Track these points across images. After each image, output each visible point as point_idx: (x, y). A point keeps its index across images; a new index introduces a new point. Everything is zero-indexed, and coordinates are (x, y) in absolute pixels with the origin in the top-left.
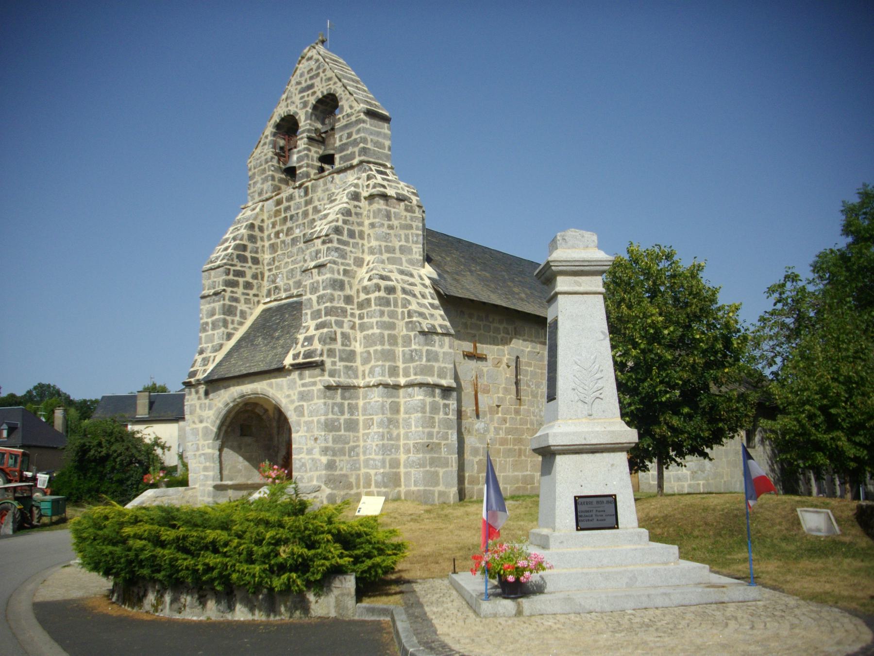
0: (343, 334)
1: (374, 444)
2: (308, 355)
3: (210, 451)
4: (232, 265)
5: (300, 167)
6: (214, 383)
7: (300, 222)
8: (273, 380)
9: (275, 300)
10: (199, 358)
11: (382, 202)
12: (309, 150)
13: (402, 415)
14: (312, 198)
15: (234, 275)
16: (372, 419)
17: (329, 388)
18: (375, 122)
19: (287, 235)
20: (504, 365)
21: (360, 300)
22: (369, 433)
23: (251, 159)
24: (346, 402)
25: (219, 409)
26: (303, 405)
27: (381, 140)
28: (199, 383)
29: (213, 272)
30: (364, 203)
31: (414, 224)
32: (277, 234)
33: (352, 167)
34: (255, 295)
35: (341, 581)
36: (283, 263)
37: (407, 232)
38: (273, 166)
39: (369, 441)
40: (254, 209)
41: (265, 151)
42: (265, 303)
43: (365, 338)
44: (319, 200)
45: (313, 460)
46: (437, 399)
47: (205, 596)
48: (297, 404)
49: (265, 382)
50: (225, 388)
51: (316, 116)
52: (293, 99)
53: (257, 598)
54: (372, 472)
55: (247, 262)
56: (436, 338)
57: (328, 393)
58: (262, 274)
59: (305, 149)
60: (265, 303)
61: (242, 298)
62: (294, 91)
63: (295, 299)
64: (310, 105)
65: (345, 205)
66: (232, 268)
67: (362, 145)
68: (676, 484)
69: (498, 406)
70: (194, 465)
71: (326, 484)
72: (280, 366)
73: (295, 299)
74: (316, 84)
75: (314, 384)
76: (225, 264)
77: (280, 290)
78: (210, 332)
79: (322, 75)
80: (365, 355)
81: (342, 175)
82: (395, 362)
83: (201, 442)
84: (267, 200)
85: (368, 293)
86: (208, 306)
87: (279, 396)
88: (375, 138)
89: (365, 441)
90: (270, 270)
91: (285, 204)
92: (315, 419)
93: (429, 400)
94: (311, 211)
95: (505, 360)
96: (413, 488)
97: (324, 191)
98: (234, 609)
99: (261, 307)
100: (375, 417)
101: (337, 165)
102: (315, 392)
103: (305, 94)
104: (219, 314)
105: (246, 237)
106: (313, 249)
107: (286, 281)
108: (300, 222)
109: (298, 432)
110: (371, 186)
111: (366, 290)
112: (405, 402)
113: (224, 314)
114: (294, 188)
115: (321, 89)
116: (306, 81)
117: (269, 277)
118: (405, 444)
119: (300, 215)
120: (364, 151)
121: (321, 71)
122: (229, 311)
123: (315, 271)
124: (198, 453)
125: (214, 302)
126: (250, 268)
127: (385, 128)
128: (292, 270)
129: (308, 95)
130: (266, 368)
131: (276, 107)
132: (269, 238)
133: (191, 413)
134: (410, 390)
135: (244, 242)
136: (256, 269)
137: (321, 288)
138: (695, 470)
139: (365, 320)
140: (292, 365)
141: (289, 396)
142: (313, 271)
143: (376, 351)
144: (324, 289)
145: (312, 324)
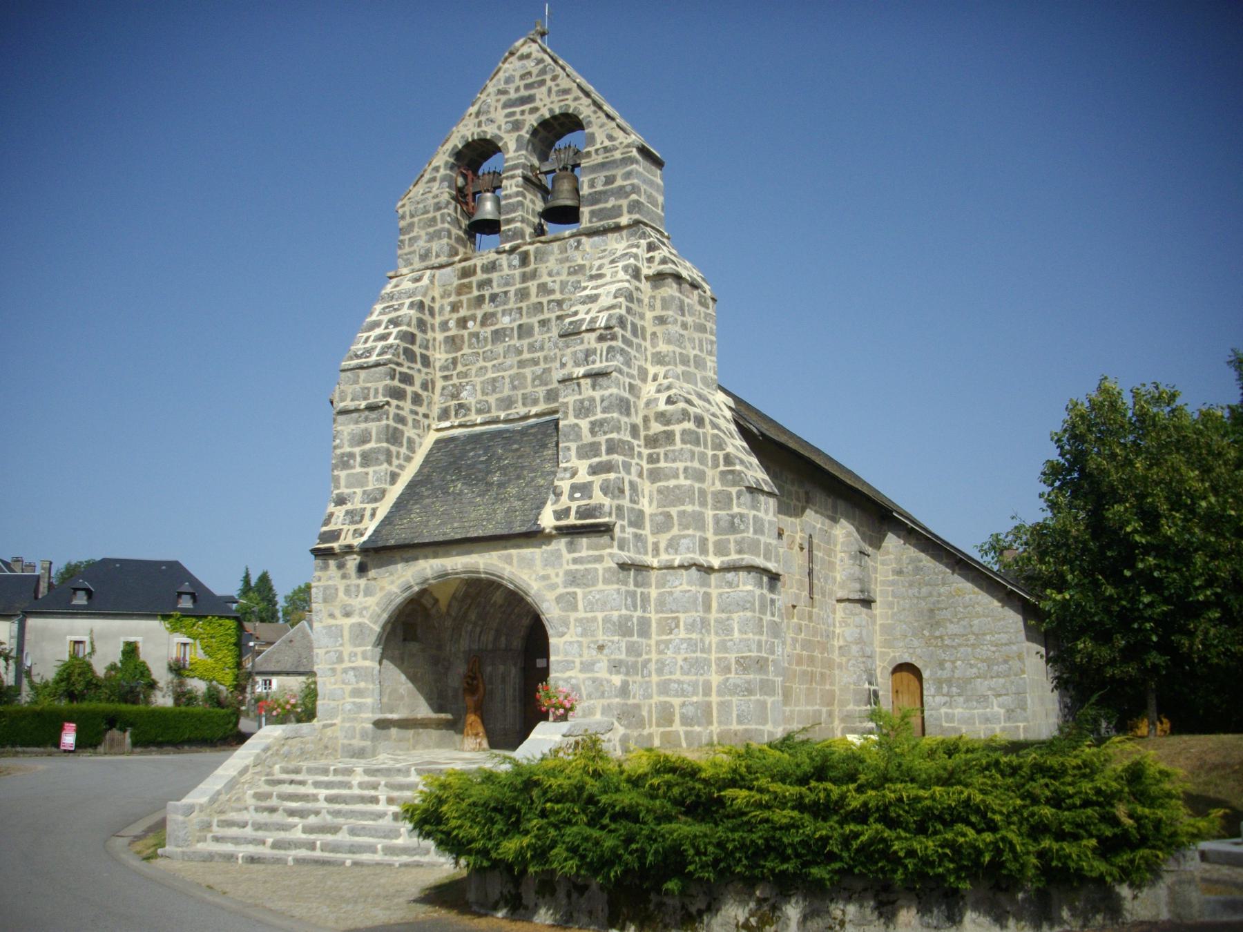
0: (631, 482)
1: (680, 658)
2: (582, 514)
3: (368, 663)
4: (398, 364)
5: (509, 222)
6: (377, 554)
7: (511, 305)
8: (514, 552)
9: (461, 426)
10: (340, 512)
11: (675, 286)
12: (525, 197)
13: (714, 615)
14: (536, 270)
15: (400, 381)
16: (677, 618)
17: (623, 567)
18: (648, 164)
19: (483, 323)
20: (797, 548)
21: (651, 432)
22: (670, 641)
23: (405, 201)
24: (639, 590)
25: (390, 593)
26: (575, 593)
27: (654, 193)
28: (349, 549)
29: (363, 374)
30: (645, 286)
31: (709, 325)
32: (462, 323)
33: (618, 228)
34: (426, 416)
35: (1177, 861)
36: (474, 369)
37: (701, 335)
38: (449, 215)
39: (669, 653)
40: (417, 280)
41: (435, 190)
42: (438, 430)
43: (659, 491)
44: (550, 274)
45: (594, 680)
46: (765, 591)
47: (893, 903)
48: (561, 590)
49: (495, 554)
50: (407, 561)
51: (533, 145)
52: (492, 115)
53: (1013, 900)
54: (676, 701)
55: (415, 362)
56: (762, 498)
57: (622, 575)
58: (433, 382)
59: (518, 194)
60: (438, 430)
61: (410, 418)
62: (493, 104)
63: (501, 426)
64: (527, 127)
65: (626, 285)
66: (398, 369)
67: (634, 197)
68: (983, 727)
69: (794, 607)
70: (330, 687)
71: (619, 719)
72: (534, 528)
73: (501, 426)
74: (538, 97)
75: (599, 559)
76: (390, 361)
77: (469, 410)
78: (358, 470)
79: (549, 83)
80: (660, 518)
81: (596, 239)
82: (704, 531)
83: (347, 649)
84: (441, 267)
85: (668, 423)
86: (352, 426)
87: (525, 577)
88: (649, 190)
89: (661, 652)
90: (446, 378)
91: (481, 276)
92: (600, 616)
93: (758, 592)
94: (533, 290)
95: (798, 540)
96: (735, 726)
97: (561, 261)
98: (961, 922)
99: (432, 437)
100: (682, 616)
101: (585, 222)
102: (601, 572)
103: (518, 109)
104: (379, 440)
105: (414, 322)
106: (579, 348)
107: (480, 397)
108: (511, 305)
109: (562, 635)
110: (657, 260)
111: (662, 417)
112: (721, 595)
113: (388, 441)
114: (498, 252)
115: (547, 105)
116: (517, 89)
117: (444, 388)
118: (719, 659)
119: (512, 294)
120: (635, 206)
121: (548, 77)
122: (394, 437)
123: (586, 383)
124: (339, 667)
125: (366, 420)
126: (419, 371)
127: (657, 177)
128: (494, 380)
129: (523, 113)
130: (499, 532)
131: (456, 124)
132: (444, 326)
133: (325, 601)
134: (730, 576)
135: (413, 330)
136: (427, 374)
137: (599, 409)
138: (1012, 707)
139: (662, 464)
140: (557, 528)
141: (545, 578)
142: (582, 381)
143: (682, 514)
144: (604, 412)
145: (583, 466)
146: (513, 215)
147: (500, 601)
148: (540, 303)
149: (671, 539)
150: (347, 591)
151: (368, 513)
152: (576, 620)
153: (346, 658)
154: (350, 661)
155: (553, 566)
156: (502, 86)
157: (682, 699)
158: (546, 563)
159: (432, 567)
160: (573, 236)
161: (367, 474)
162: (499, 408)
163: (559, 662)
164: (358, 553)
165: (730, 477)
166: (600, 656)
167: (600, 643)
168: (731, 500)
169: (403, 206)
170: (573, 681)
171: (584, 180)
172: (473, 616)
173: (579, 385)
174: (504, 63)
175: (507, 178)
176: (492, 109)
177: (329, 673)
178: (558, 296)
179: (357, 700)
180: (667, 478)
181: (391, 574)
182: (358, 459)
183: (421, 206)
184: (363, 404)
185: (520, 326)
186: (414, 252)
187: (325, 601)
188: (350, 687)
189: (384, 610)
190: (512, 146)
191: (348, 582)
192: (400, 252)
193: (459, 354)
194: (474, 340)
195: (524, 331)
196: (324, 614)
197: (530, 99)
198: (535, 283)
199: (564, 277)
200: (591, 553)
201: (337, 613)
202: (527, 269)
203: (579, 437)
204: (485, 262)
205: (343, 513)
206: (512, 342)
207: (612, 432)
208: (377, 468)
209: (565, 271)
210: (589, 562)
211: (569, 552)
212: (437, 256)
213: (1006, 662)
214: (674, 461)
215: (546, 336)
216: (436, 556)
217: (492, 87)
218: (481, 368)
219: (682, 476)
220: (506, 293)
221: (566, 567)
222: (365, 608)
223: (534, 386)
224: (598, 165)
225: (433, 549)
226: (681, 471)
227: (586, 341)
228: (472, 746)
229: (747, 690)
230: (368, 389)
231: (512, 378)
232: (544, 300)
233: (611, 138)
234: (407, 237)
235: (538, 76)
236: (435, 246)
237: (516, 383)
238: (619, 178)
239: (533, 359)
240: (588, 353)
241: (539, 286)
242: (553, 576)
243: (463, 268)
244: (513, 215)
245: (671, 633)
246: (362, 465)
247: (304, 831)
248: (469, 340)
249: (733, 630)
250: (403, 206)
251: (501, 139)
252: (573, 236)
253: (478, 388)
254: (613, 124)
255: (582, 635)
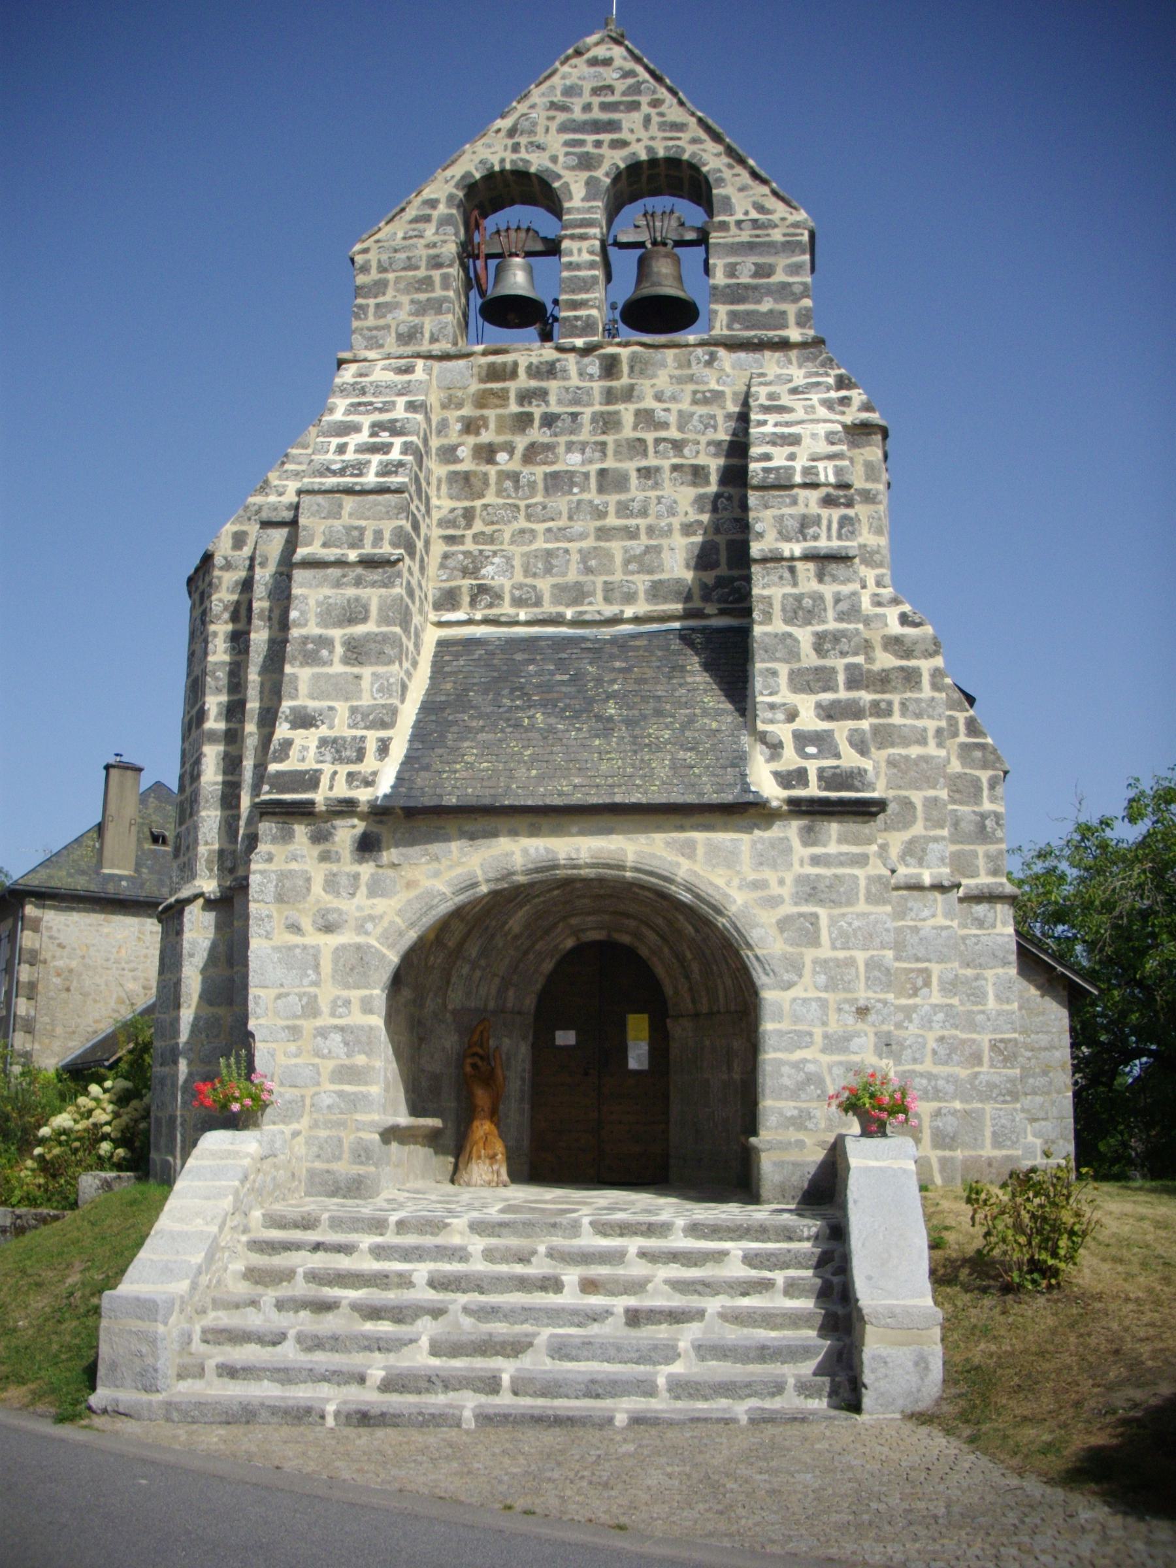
5: (575, 305)
7: (585, 435)
8: (699, 836)
9: (486, 621)
14: (632, 388)
22: (915, 1008)
25: (429, 894)
26: (816, 916)
28: (346, 807)
29: (349, 502)
32: (487, 453)
33: (784, 345)
39: (913, 1028)
42: (440, 624)
44: (659, 397)
48: (788, 909)
49: (659, 838)
50: (472, 837)
52: (540, 138)
64: (606, 166)
70: (282, 1060)
75: (861, 860)
78: (338, 668)
79: (645, 109)
83: (327, 993)
84: (445, 357)
85: (908, 654)
86: (327, 591)
87: (720, 882)
90: (450, 540)
91: (523, 381)
92: (861, 956)
96: (988, 1151)
97: (680, 380)
100: (936, 969)
102: (862, 883)
106: (787, 511)
107: (519, 577)
109: (789, 986)
115: (642, 139)
117: (446, 556)
119: (586, 418)
124: (308, 1025)
125: (358, 582)
128: (549, 553)
129: (598, 144)
131: (471, 138)
133: (280, 899)
134: (980, 909)
138: (1053, 1136)
139: (896, 719)
141: (758, 885)
142: (799, 565)
146: (585, 296)
147: (516, 929)
148: (641, 441)
149: (912, 842)
150: (331, 884)
151: (371, 747)
152: (815, 962)
153: (325, 1007)
154: (333, 1015)
155: (774, 866)
156: (558, 98)
157: (935, 1105)
158: (761, 861)
159: (525, 851)
160: (702, 344)
161: (358, 677)
162: (556, 601)
163: (781, 1033)
164: (362, 817)
165: (978, 754)
166: (860, 1026)
167: (861, 1003)
168: (981, 789)
169: (365, 251)
170: (810, 1068)
171: (719, 263)
172: (473, 950)
173: (792, 570)
174: (563, 64)
175: (572, 237)
176: (540, 129)
177: (283, 1035)
178: (673, 433)
179: (347, 1088)
180: (906, 742)
181: (437, 859)
182: (339, 650)
183: (402, 256)
184: (353, 556)
185: (602, 473)
186: (388, 327)
187: (280, 899)
188: (330, 1064)
189: (412, 925)
190: (578, 191)
191: (334, 868)
192: (356, 324)
193: (478, 503)
194: (508, 484)
195: (608, 481)
196: (278, 923)
197: (612, 126)
198: (632, 407)
199: (685, 405)
200: (845, 848)
201: (306, 923)
202: (614, 383)
203: (793, 654)
204: (535, 360)
205: (313, 744)
206: (586, 496)
207: (856, 654)
208: (381, 669)
209: (688, 398)
210: (842, 864)
211: (806, 844)
212: (434, 339)
213: (1045, 1073)
214: (918, 716)
215: (653, 494)
216: (534, 832)
217: (538, 95)
218: (522, 531)
219: (932, 742)
220: (574, 416)
221: (797, 869)
222: (371, 918)
223: (627, 572)
224: (742, 244)
225: (531, 819)
226: (931, 733)
227: (801, 500)
228: (487, 1178)
229: (1010, 1093)
230: (361, 530)
231: (585, 556)
232: (650, 437)
233: (761, 209)
234: (372, 302)
235: (624, 94)
236: (429, 323)
237: (593, 563)
238: (779, 270)
239: (626, 528)
240: (805, 524)
241: (638, 413)
242: (773, 883)
243: (492, 365)
244: (585, 296)
245: (915, 994)
246: (346, 661)
247: (435, 1351)
248: (499, 482)
249: (985, 995)
250: (365, 251)
251: (559, 177)
252: (702, 344)
253: (517, 562)
254: (765, 190)
255: (826, 989)
